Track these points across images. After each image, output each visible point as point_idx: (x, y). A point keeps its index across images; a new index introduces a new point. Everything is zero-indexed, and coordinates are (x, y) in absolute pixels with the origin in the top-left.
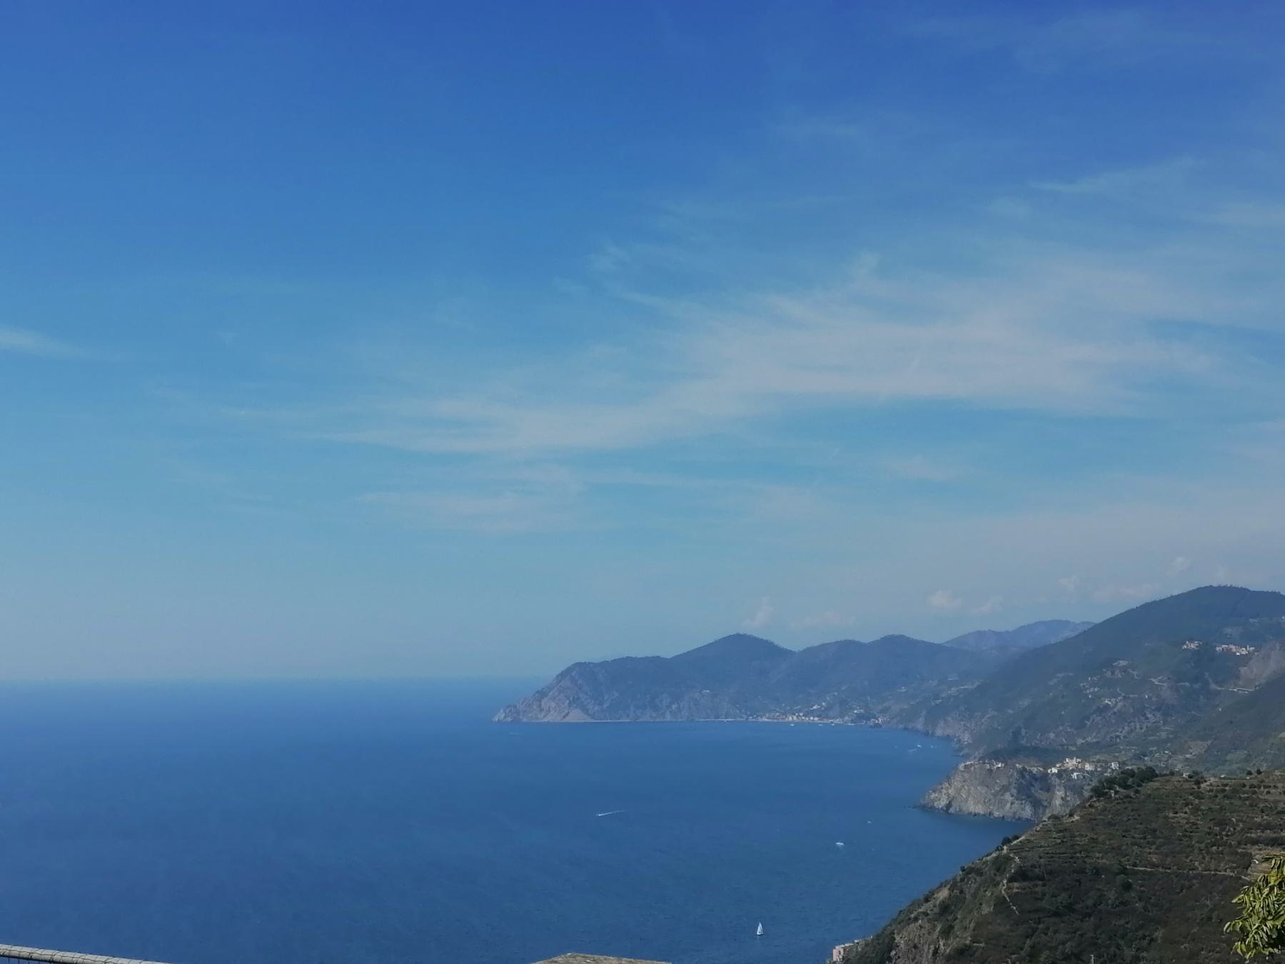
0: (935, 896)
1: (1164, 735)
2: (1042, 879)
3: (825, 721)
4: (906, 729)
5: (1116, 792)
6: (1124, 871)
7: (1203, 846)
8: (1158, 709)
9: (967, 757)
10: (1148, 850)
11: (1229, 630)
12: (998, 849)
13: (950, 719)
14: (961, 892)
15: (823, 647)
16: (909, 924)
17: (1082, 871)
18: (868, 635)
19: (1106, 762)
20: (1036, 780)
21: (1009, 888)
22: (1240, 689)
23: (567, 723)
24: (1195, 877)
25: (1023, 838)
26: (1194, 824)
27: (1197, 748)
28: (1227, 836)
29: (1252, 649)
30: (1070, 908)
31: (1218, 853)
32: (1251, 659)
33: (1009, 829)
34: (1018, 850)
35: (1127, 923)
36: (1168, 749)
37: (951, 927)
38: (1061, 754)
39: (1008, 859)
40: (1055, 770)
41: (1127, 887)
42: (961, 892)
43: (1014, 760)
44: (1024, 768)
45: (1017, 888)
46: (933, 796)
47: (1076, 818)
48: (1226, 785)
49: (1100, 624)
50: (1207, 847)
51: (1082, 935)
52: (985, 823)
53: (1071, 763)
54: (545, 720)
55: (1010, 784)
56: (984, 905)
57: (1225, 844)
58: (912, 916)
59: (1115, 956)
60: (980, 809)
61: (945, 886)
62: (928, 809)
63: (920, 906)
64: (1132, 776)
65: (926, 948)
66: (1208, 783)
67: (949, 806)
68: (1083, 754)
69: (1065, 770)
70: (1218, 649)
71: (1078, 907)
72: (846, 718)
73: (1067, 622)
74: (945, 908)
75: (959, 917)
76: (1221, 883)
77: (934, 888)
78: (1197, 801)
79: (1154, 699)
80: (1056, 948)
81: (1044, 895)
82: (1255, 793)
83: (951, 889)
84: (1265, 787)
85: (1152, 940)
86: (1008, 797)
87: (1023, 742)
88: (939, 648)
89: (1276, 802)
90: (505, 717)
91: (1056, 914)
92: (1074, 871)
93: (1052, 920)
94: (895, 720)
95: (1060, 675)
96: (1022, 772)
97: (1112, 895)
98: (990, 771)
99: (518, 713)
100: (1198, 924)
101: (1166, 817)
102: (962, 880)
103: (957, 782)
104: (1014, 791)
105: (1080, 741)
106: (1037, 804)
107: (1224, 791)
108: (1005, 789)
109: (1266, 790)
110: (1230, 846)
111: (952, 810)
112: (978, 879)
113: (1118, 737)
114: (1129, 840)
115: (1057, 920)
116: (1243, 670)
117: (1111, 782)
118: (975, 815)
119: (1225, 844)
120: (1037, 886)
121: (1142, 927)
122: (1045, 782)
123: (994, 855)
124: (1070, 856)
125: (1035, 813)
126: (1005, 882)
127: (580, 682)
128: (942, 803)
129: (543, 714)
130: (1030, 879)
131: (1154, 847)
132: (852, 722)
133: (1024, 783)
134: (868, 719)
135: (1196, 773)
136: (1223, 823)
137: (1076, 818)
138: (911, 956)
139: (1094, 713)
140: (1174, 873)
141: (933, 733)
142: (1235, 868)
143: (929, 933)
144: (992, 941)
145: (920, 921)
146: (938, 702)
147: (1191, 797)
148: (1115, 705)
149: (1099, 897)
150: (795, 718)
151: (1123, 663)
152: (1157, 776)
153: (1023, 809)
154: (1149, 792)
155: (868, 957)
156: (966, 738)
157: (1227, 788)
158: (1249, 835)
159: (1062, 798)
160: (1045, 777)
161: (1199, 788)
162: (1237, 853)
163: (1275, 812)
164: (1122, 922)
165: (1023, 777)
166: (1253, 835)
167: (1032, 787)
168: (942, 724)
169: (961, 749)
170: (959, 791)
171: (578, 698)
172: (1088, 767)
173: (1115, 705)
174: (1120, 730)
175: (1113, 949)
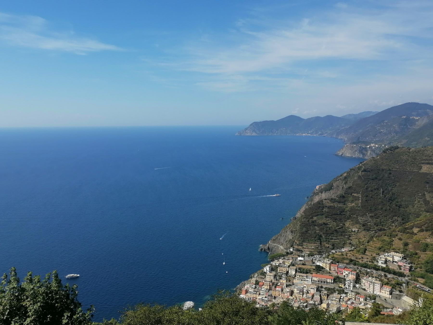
0: (343, 175)
1: (396, 138)
2: (370, 172)
3: (312, 135)
4: (331, 137)
5: (389, 152)
6: (390, 170)
7: (409, 164)
8: (395, 132)
9: (346, 144)
10: (396, 165)
11: (413, 113)
12: (359, 165)
14: (350, 174)
15: (312, 118)
16: (337, 181)
17: (379, 170)
18: (323, 115)
19: (381, 145)
20: (364, 149)
21: (361, 173)
22: (416, 127)
24: (407, 171)
25: (365, 162)
26: (408, 159)
27: (404, 141)
28: (416, 162)
29: (419, 117)
30: (376, 178)
31: (414, 166)
32: (419, 120)
33: (361, 160)
34: (364, 165)
35: (390, 182)
36: (397, 142)
37: (347, 182)
38: (370, 143)
39: (361, 167)
40: (368, 147)
41: (390, 174)
42: (350, 174)
43: (359, 144)
44: (361, 146)
45: (363, 173)
46: (338, 152)
47: (378, 158)
48: (417, 150)
50: (410, 164)
51: (379, 184)
52: (351, 159)
53: (372, 145)
54: (247, 135)
56: (355, 177)
57: (415, 164)
58: (338, 179)
59: (386, 189)
60: (349, 155)
61: (346, 173)
62: (337, 155)
63: (339, 177)
66: (412, 150)
67: (342, 155)
68: (376, 143)
69: (371, 147)
70: (411, 118)
72: (317, 134)
73: (372, 112)
74: (345, 178)
75: (349, 180)
76: (414, 173)
77: (343, 173)
78: (409, 154)
79: (394, 130)
80: (373, 187)
81: (370, 175)
82: (424, 152)
83: (347, 173)
84: (426, 151)
85: (396, 186)
86: (357, 153)
87: (360, 140)
88: (340, 118)
89: (429, 154)
90: (238, 134)
91: (373, 180)
92: (377, 170)
93: (372, 181)
94: (329, 135)
96: (360, 147)
97: (386, 175)
98: (353, 147)
99: (241, 133)
100: (408, 182)
101: (401, 158)
102: (350, 172)
103: (344, 149)
104: (358, 151)
105: (374, 140)
106: (364, 154)
107: (416, 151)
108: (356, 151)
109: (427, 151)
110: (417, 164)
111: (343, 156)
112: (354, 171)
114: (391, 163)
115: (373, 181)
116: (417, 123)
117: (387, 149)
118: (348, 157)
119: (415, 164)
120: (368, 173)
121: (393, 182)
122: (366, 149)
123: (358, 166)
124: (376, 166)
125: (363, 157)
126: (360, 172)
127: (255, 126)
128: (341, 154)
129: (247, 133)
130: (367, 172)
132: (318, 135)
134: (322, 135)
135: (409, 147)
137: (378, 158)
138: (337, 188)
139: (379, 133)
141: (338, 138)
142: (418, 169)
143: (341, 183)
144: (357, 185)
145: (339, 181)
146: (339, 131)
147: (407, 153)
148: (384, 131)
149: (383, 176)
150: (305, 134)
151: (386, 121)
152: (399, 148)
153: (360, 155)
154: (397, 152)
155: (327, 188)
157: (417, 151)
158: (422, 162)
159: (370, 153)
160: (366, 148)
161: (410, 151)
162: (418, 166)
163: (429, 156)
164: (389, 181)
165: (361, 148)
166: (423, 162)
167: (363, 151)
168: (340, 136)
169: (345, 142)
171: (255, 130)
172: (377, 146)
173: (384, 131)
174: (385, 137)
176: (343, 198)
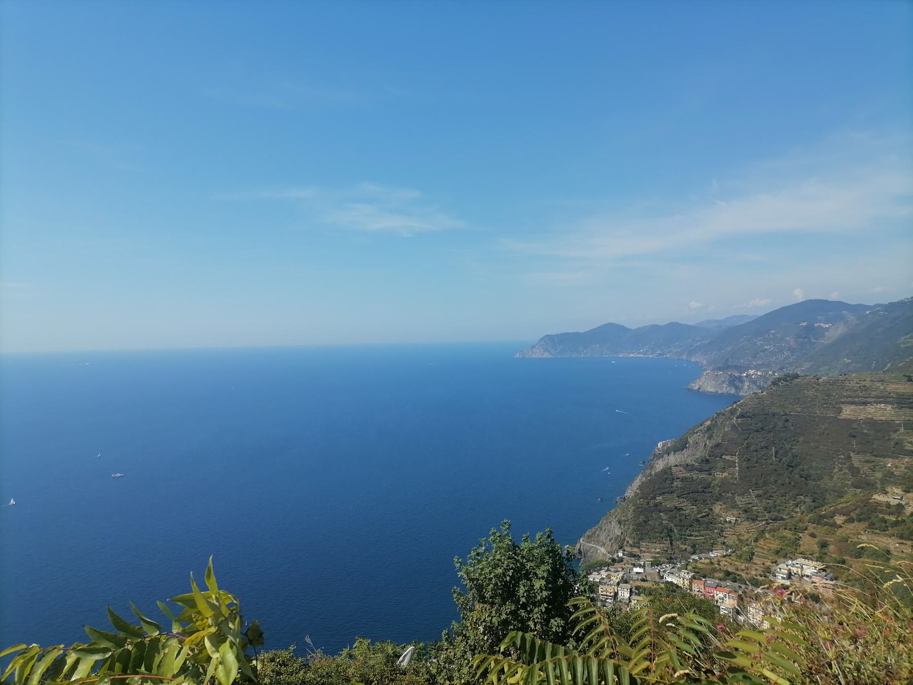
1: (791, 360)
2: (751, 417)
5: (782, 383)
7: (820, 404)
8: (789, 350)
9: (705, 370)
10: (796, 406)
11: (819, 317)
13: (698, 355)
17: (767, 414)
23: (543, 358)
34: (740, 406)
37: (712, 436)
38: (748, 368)
39: (736, 409)
40: (745, 375)
41: (787, 421)
44: (732, 374)
46: (693, 385)
47: (764, 393)
48: (831, 380)
49: (763, 316)
53: (751, 372)
55: (726, 380)
60: (713, 390)
62: (691, 390)
64: (789, 377)
65: (701, 443)
67: (699, 388)
68: (757, 368)
71: (765, 428)
75: (715, 432)
78: (817, 387)
80: (758, 444)
82: (843, 383)
84: (848, 381)
86: (724, 385)
87: (730, 364)
91: (757, 431)
93: (756, 433)
95: (745, 337)
96: (731, 376)
97: (780, 424)
98: (717, 375)
101: (804, 393)
102: (716, 418)
103: (703, 379)
105: (754, 363)
106: (737, 388)
108: (723, 382)
110: (832, 404)
111: (700, 390)
112: (723, 417)
113: (771, 361)
115: (757, 433)
116: (826, 334)
120: (748, 420)
123: (730, 408)
125: (736, 392)
128: (697, 387)
131: (798, 405)
133: (731, 379)
136: (829, 396)
140: (807, 415)
143: (702, 438)
147: (815, 385)
148: (770, 349)
149: (775, 424)
151: (773, 332)
156: (705, 362)
164: (785, 434)
165: (731, 377)
166: (843, 400)
167: (735, 382)
168: (694, 357)
169: (703, 367)
170: (704, 383)
172: (759, 373)
173: (770, 349)
175: (781, 445)
176: (706, 464)
